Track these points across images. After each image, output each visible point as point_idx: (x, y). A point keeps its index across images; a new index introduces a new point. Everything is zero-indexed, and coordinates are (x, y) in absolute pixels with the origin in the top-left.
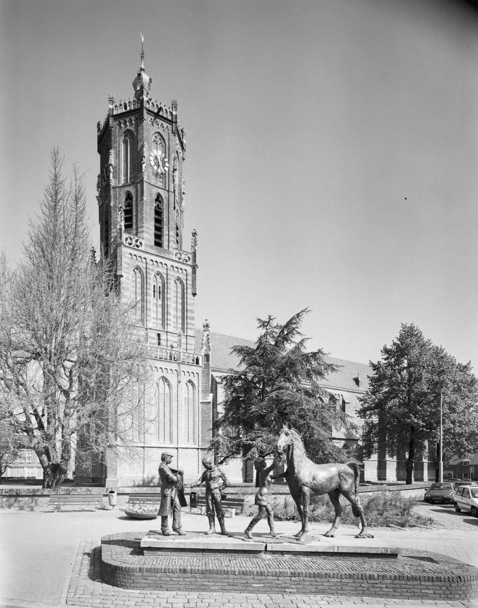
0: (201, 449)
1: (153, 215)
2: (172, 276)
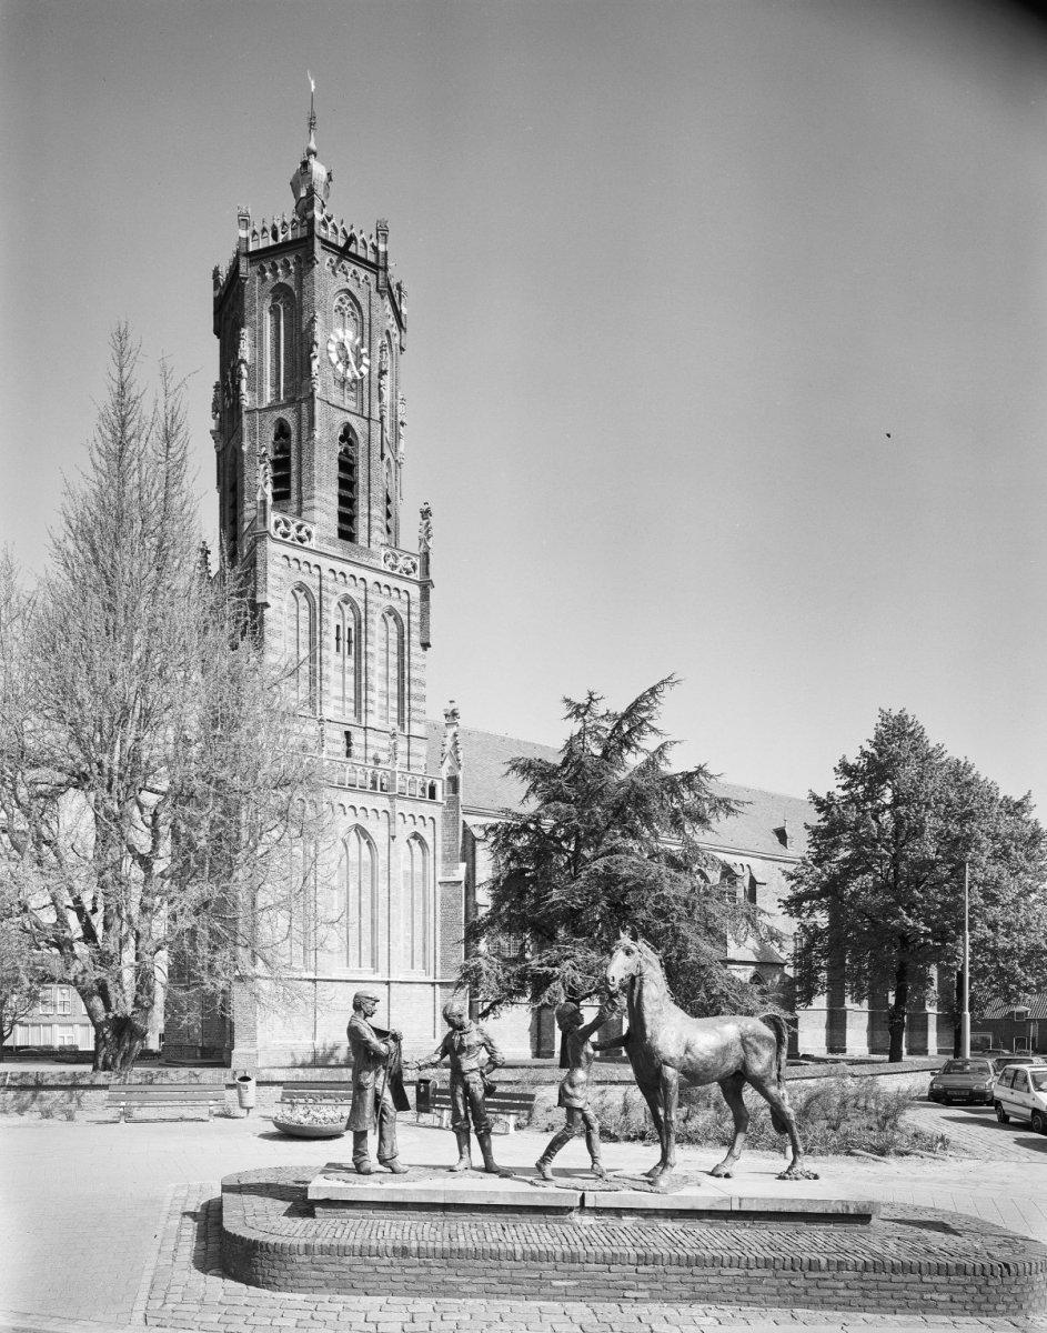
0: (441, 984)
1: (335, 471)
2: (378, 605)
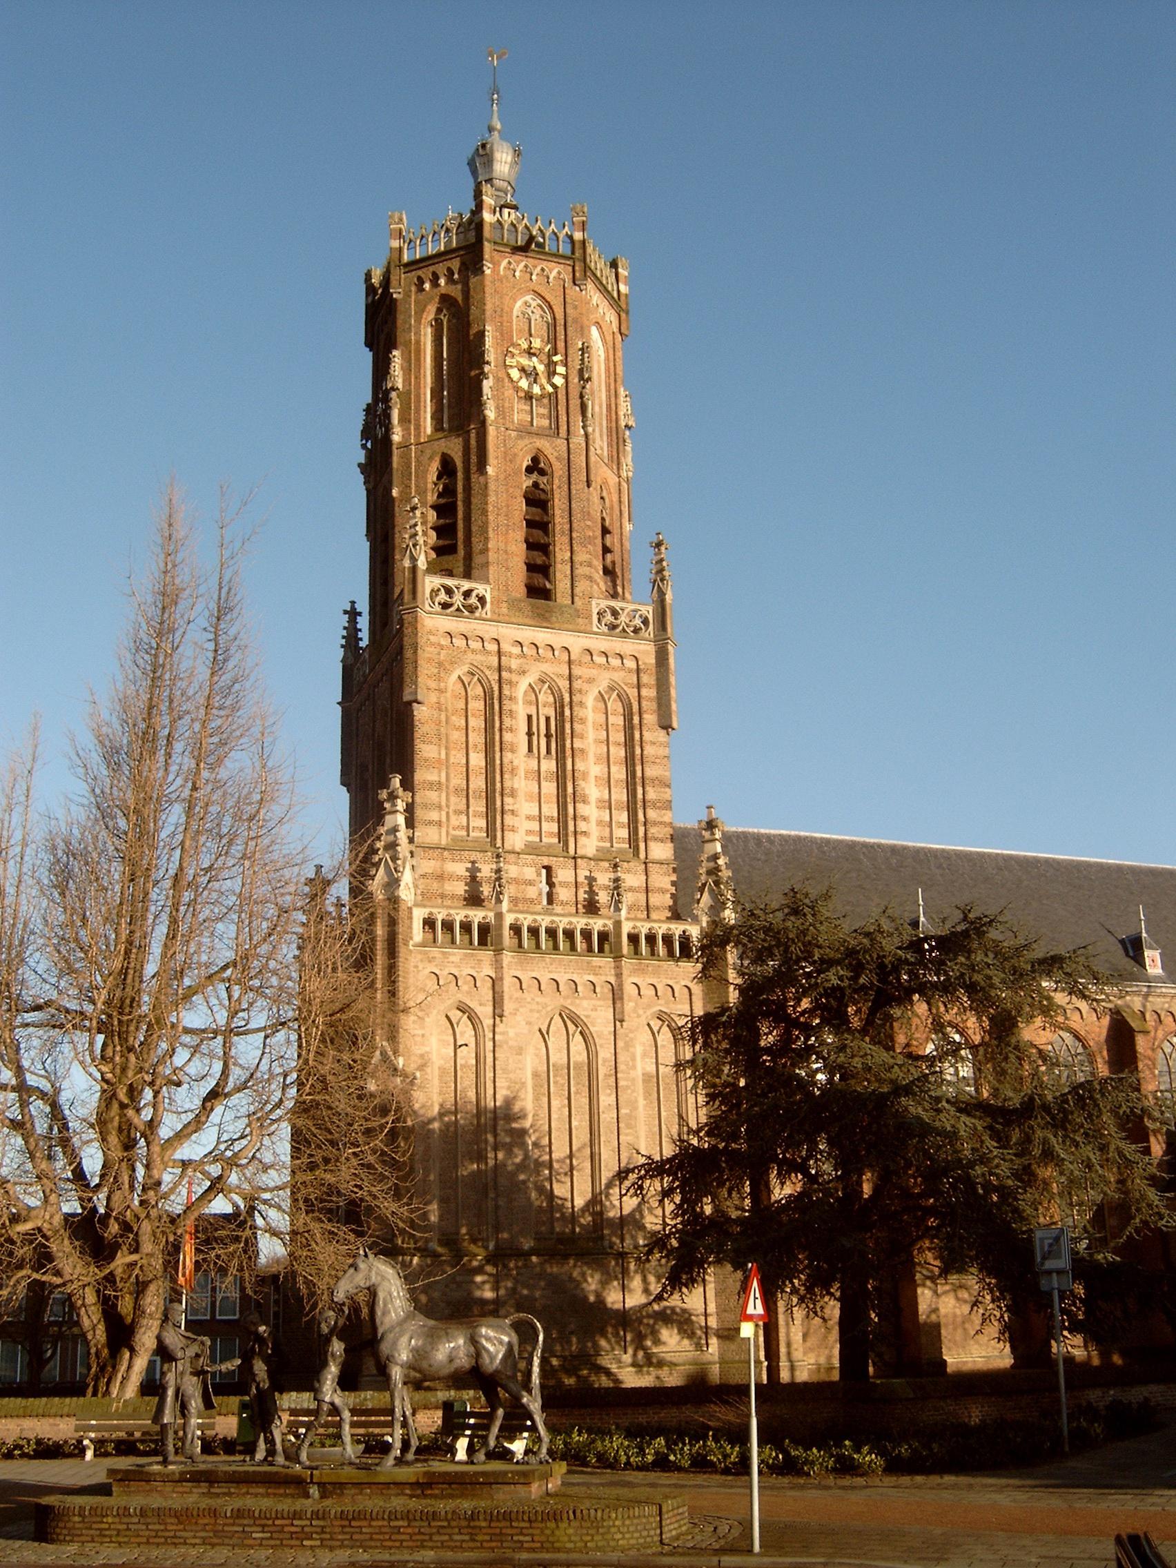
1: (520, 507)
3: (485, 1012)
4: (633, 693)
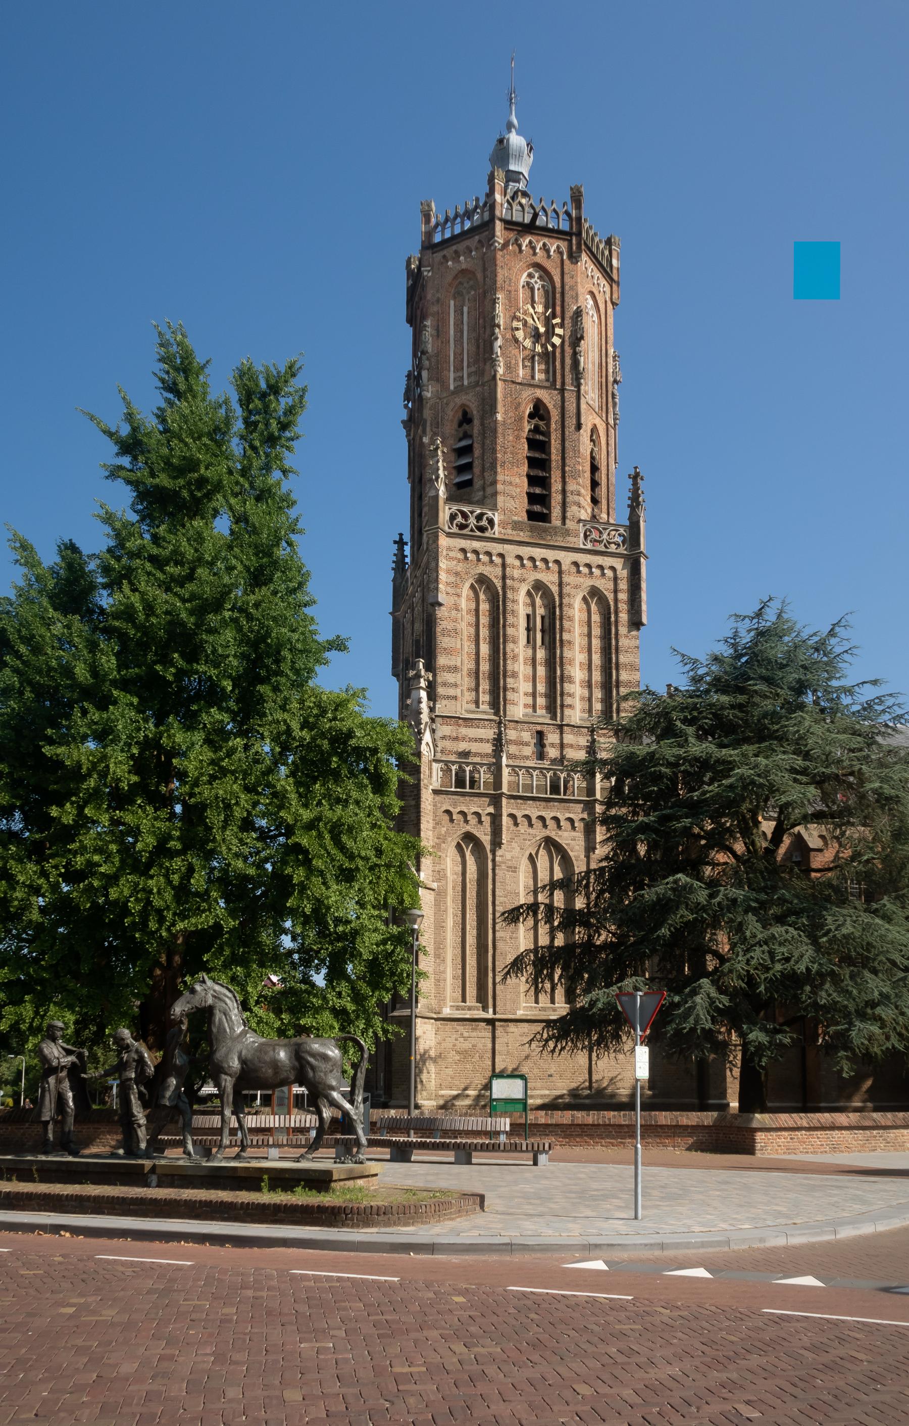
1: (524, 448)
3: (486, 839)
4: (610, 597)
